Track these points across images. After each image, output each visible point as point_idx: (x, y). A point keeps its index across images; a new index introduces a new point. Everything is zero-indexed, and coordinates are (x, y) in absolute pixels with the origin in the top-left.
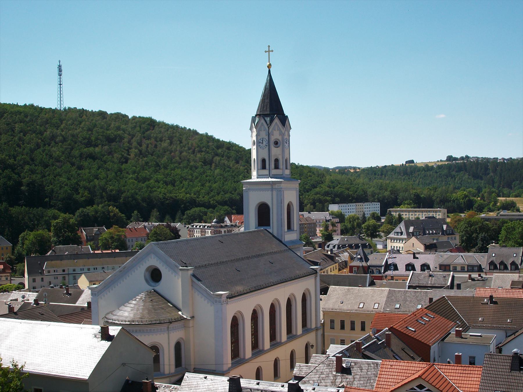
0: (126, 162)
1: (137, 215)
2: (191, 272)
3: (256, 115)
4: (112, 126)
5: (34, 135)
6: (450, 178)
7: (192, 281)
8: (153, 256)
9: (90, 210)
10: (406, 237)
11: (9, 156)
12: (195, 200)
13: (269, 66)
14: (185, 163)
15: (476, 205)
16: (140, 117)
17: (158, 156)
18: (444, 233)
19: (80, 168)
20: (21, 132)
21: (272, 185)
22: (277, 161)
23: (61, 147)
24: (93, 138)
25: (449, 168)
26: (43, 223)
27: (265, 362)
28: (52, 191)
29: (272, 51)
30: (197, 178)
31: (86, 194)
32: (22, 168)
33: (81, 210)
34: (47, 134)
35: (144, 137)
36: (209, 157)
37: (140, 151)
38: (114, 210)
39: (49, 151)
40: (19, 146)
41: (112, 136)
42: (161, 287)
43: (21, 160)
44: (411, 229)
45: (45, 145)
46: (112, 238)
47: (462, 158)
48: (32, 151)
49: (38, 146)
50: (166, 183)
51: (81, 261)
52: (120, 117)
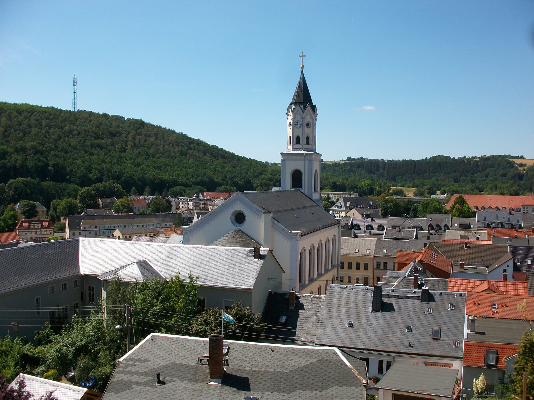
0: (125, 151)
1: (135, 190)
2: (271, 215)
3: (292, 104)
4: (114, 124)
5: (57, 129)
6: (351, 173)
7: (272, 222)
8: (239, 203)
9: (100, 185)
10: (344, 209)
11: (39, 143)
12: (176, 181)
13: (302, 67)
14: (167, 154)
15: (376, 191)
16: (133, 119)
17: (148, 148)
18: (371, 207)
19: (92, 154)
20: (47, 126)
21: (305, 157)
22: (308, 138)
23: (77, 138)
24: (100, 133)
25: (351, 165)
26: (66, 194)
27: (314, 286)
28: (72, 171)
29: (305, 56)
30: (176, 165)
31: (97, 173)
32: (49, 153)
33: (94, 185)
34: (66, 128)
35: (137, 134)
36: (184, 150)
37: (135, 144)
38: (118, 186)
39: (69, 141)
40: (45, 136)
41: (114, 132)
42: (245, 227)
43: (47, 147)
44: (348, 204)
45: (65, 137)
46: (123, 205)
47: (358, 159)
48: (56, 141)
49: (60, 137)
50: (155, 168)
51: (109, 221)
52: (118, 119)
